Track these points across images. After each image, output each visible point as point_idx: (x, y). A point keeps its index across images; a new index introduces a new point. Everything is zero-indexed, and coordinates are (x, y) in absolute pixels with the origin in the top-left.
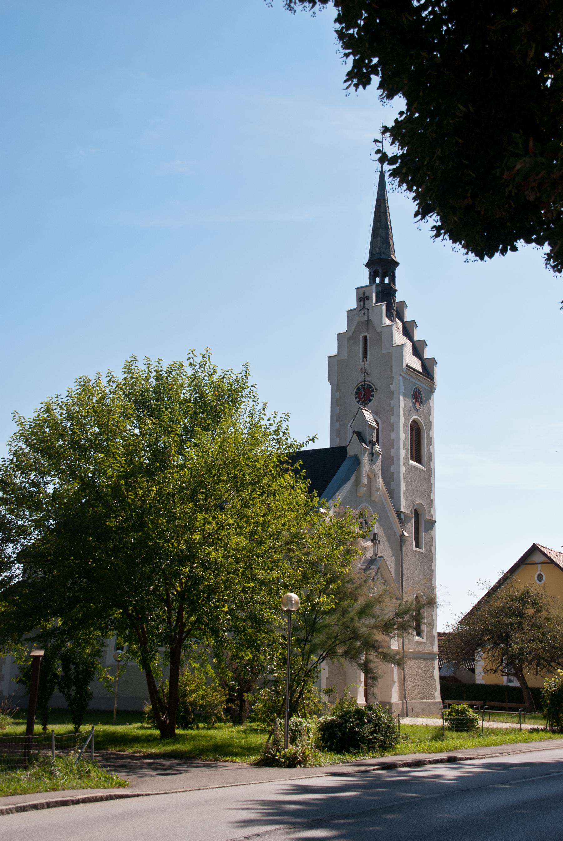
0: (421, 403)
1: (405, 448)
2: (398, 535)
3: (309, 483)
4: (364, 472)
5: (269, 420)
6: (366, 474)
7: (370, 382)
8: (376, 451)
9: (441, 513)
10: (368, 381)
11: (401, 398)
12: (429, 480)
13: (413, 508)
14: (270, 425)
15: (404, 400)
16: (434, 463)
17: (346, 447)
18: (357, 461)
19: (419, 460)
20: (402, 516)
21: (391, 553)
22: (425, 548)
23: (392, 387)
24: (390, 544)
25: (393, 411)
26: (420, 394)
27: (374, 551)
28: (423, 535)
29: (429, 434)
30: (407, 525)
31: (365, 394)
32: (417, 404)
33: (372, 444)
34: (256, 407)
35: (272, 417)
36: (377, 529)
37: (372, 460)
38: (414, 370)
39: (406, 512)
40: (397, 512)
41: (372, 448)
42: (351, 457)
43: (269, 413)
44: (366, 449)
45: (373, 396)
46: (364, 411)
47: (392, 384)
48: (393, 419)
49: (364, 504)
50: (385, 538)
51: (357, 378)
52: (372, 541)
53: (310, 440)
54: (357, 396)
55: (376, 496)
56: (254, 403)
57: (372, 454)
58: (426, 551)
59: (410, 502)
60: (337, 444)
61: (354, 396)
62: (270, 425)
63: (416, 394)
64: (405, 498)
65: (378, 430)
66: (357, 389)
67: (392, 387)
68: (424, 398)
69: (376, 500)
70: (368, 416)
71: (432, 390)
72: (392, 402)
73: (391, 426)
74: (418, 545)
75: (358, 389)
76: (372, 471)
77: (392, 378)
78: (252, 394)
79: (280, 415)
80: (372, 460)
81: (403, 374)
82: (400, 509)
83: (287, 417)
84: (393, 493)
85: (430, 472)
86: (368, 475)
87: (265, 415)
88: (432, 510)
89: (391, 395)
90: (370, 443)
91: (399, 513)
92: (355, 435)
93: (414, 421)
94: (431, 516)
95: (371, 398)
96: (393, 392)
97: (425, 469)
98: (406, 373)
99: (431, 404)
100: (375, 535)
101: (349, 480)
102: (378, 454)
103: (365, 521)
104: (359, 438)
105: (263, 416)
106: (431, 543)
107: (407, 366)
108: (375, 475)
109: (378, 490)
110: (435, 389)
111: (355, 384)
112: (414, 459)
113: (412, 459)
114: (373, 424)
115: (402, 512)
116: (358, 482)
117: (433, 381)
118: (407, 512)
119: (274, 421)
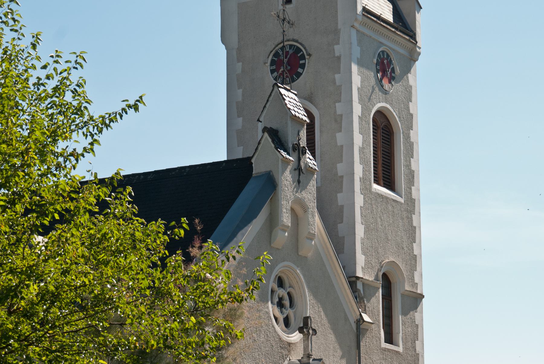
0: (391, 79)
1: (363, 161)
2: (352, 320)
3: (130, 194)
4: (284, 202)
5: (45, 67)
6: (289, 208)
7: (297, 41)
8: (306, 164)
9: (431, 280)
10: (294, 40)
11: (355, 68)
12: (411, 220)
13: (379, 270)
14: (48, 77)
15: (360, 73)
16: (419, 190)
17: (250, 159)
18: (270, 184)
19: (390, 184)
20: (359, 286)
21: (339, 353)
22: (405, 343)
23: (338, 49)
24: (336, 337)
25: (341, 92)
26: (390, 62)
27: (306, 348)
28: (399, 320)
29: (407, 137)
30: (369, 301)
31: (289, 64)
32: (385, 82)
33: (299, 151)
34: (19, 42)
35: (51, 61)
36: (310, 306)
37: (299, 182)
38: (379, 17)
39: (366, 277)
40: (349, 277)
41: (299, 159)
42: (260, 176)
43: (45, 51)
44: (286, 162)
45: (303, 66)
46: (283, 91)
47: (338, 43)
48: (340, 108)
49: (286, 263)
50: (327, 325)
51: (271, 37)
52: (301, 330)
53: (130, 107)
54: (274, 67)
55: (308, 250)
56: (15, 35)
57: (298, 170)
58: (405, 348)
59: (374, 261)
60: (239, 154)
61: (268, 68)
62: (48, 77)
63: (383, 63)
64: (364, 253)
65: (311, 128)
66: (274, 56)
67: (338, 49)
68: (398, 70)
69: (310, 255)
70: (291, 98)
71: (413, 56)
72: (337, 76)
73: (336, 121)
74: (389, 339)
75: (276, 55)
76: (300, 202)
77: (336, 32)
78: (10, 16)
79: (66, 56)
80: (299, 182)
81: (356, 25)
82: (355, 271)
83: (79, 62)
84: (342, 244)
85: (411, 206)
86: (292, 209)
87: (38, 58)
88: (416, 274)
89: (336, 64)
90: (294, 149)
91: (353, 281)
92: (266, 135)
93: (379, 113)
94: (415, 285)
95: (300, 70)
96: (339, 58)
97: (402, 200)
98: (364, 24)
99: (411, 82)
100: (306, 320)
101: (255, 217)
102: (311, 171)
103: (289, 294)
104: (273, 141)
105: (35, 62)
106: (415, 334)
107: (364, 9)
108: (305, 209)
109: (311, 237)
110: (419, 54)
111: (271, 46)
112: (382, 182)
113: (377, 182)
114: (302, 114)
115: (358, 278)
116: (273, 221)
117: (415, 39)
118: (369, 277)
119: (55, 69)
